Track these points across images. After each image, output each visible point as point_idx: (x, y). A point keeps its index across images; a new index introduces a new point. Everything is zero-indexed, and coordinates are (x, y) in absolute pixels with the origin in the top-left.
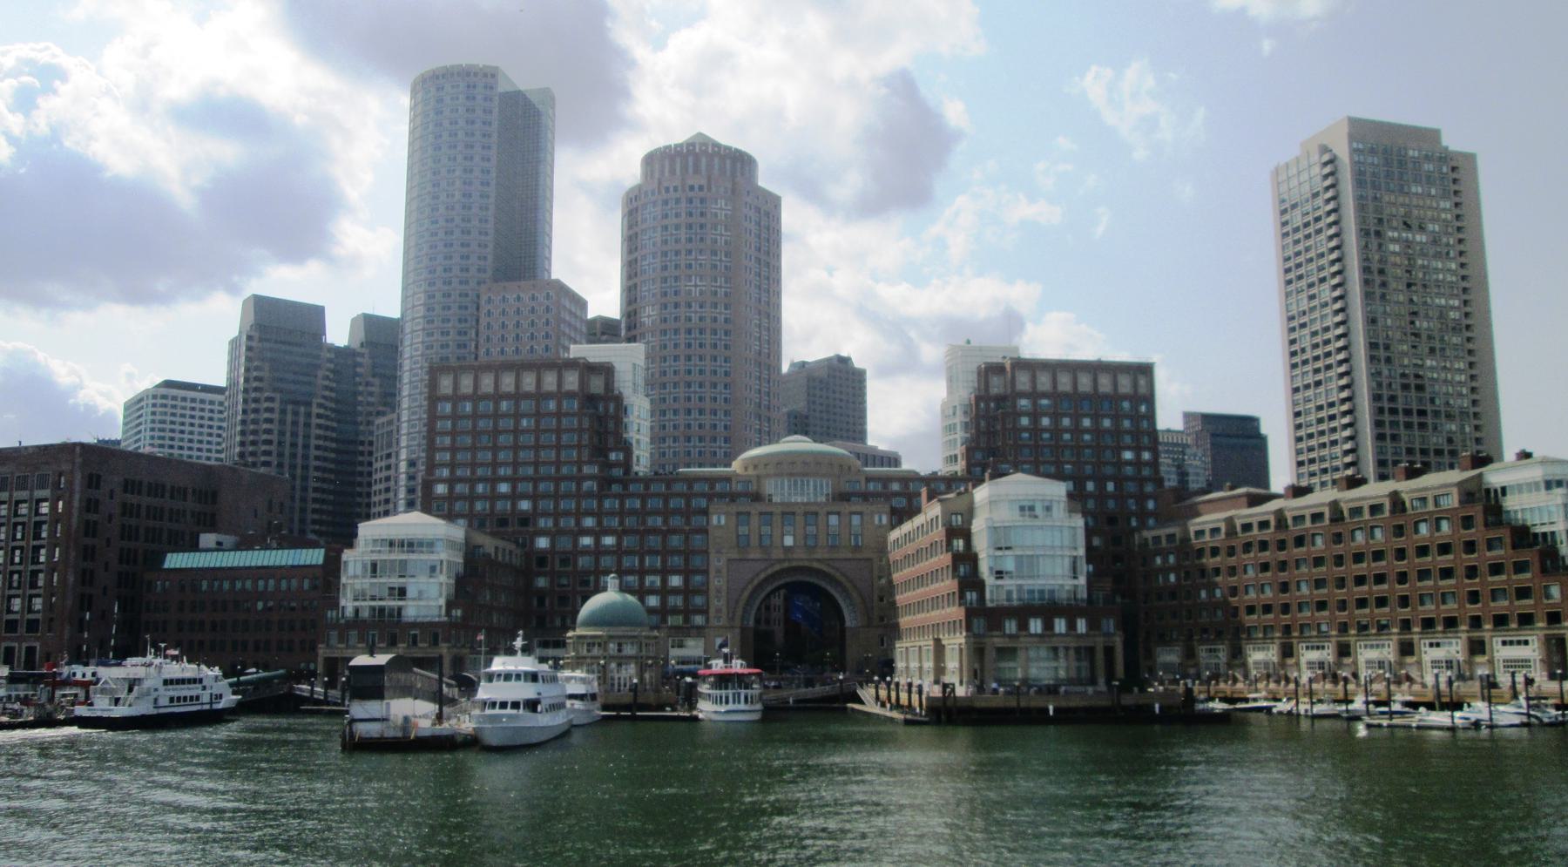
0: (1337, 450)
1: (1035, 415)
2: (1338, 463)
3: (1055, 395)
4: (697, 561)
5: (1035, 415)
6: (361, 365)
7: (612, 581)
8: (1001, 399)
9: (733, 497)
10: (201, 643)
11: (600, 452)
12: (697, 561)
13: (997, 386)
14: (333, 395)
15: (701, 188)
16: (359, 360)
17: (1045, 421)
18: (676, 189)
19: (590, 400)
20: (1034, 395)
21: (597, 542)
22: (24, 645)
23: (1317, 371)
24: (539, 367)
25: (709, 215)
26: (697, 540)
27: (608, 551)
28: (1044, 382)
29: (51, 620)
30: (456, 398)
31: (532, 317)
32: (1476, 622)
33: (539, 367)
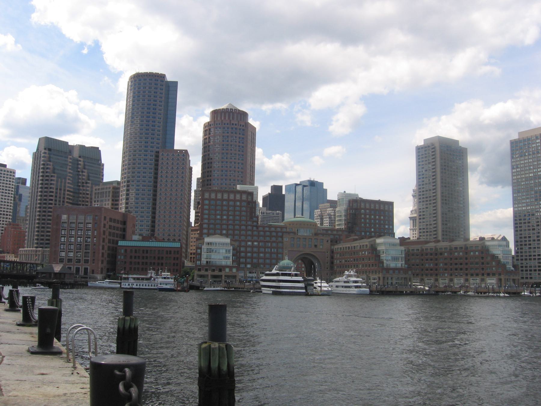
0: (432, 227)
2: (432, 230)
3: (370, 210)
4: (280, 250)
5: (365, 214)
6: (80, 164)
7: (286, 257)
8: (356, 209)
9: (289, 233)
10: (138, 268)
11: (251, 218)
12: (280, 250)
13: (355, 205)
14: (72, 175)
15: (236, 125)
16: (80, 163)
17: (368, 216)
18: (228, 124)
19: (249, 203)
20: (365, 209)
21: (253, 244)
22: (75, 267)
23: (427, 204)
24: (229, 192)
25: (231, 133)
26: (280, 245)
27: (255, 247)
28: (368, 206)
29: (94, 260)
30: (210, 199)
31: (178, 162)
32: (422, 275)
33: (229, 192)
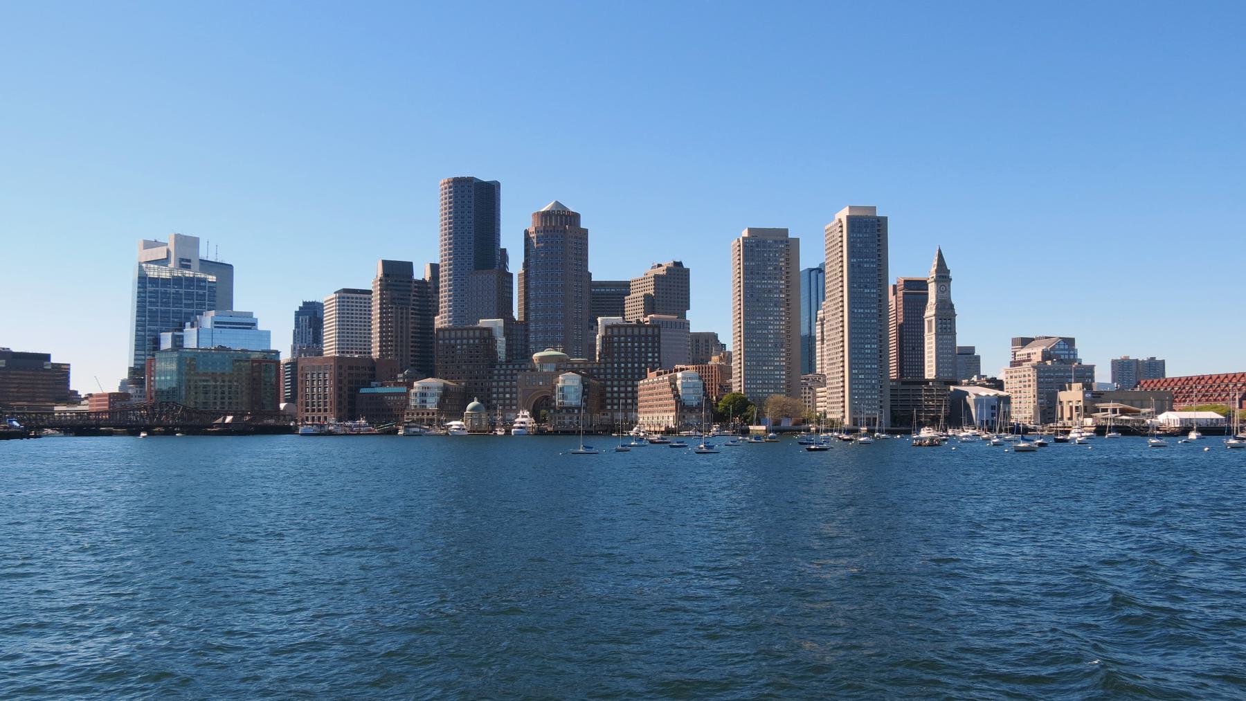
1: (619, 342)
5: (619, 342)
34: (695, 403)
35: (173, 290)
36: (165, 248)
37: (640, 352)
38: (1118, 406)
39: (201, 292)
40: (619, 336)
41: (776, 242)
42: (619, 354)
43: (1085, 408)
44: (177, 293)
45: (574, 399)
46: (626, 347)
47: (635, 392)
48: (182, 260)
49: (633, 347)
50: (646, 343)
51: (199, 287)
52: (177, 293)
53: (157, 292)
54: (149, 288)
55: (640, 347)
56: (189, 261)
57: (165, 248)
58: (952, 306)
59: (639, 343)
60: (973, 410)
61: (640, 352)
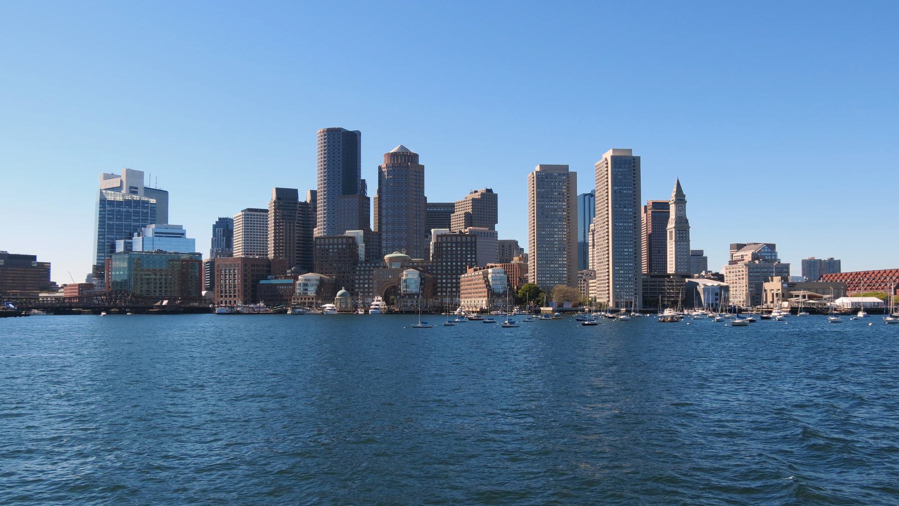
1: (447, 247)
5: (447, 247)
34: (501, 291)
35: (125, 210)
36: (119, 179)
37: (462, 254)
38: (807, 293)
39: (145, 211)
40: (447, 243)
41: (560, 174)
42: (447, 255)
43: (783, 294)
44: (128, 211)
45: (414, 288)
46: (452, 250)
47: (458, 283)
48: (131, 187)
49: (457, 250)
50: (466, 248)
51: (144, 207)
52: (128, 211)
53: (113, 211)
54: (108, 208)
55: (462, 251)
56: (136, 188)
57: (119, 179)
58: (687, 221)
59: (461, 247)
60: (702, 296)
61: (462, 254)
